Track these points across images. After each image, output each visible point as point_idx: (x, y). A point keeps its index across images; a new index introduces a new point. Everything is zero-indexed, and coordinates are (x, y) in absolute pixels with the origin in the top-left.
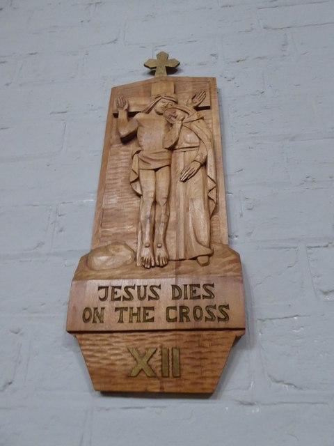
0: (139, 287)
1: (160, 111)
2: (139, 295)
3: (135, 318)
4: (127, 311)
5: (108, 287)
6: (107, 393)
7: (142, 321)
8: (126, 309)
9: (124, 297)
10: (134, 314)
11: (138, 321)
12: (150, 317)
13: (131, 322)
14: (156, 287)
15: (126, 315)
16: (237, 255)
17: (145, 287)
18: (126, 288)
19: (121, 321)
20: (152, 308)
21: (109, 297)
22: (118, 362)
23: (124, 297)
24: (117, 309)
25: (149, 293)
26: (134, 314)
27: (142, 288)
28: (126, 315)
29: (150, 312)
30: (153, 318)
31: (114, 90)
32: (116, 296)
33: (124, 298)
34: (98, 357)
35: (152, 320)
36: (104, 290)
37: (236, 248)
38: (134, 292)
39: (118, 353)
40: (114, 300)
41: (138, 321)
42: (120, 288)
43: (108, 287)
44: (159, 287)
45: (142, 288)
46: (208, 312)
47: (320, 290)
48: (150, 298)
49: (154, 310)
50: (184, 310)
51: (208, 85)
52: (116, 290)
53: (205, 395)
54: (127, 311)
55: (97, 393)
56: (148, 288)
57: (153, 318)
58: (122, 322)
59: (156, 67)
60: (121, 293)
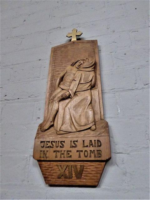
0: (56, 142)
1: (77, 67)
3: (62, 156)
4: (59, 152)
6: (51, 186)
7: (66, 157)
8: (58, 151)
9: (50, 146)
10: (62, 154)
13: (61, 157)
16: (107, 123)
19: (56, 157)
20: (71, 151)
22: (54, 174)
23: (60, 146)
24: (54, 151)
25: (60, 144)
26: (62, 154)
28: (82, 154)
29: (70, 153)
30: (71, 156)
32: (47, 146)
36: (43, 143)
37: (108, 120)
39: (57, 170)
41: (64, 157)
42: (49, 142)
44: (77, 141)
47: (96, 60)
48: (61, 147)
50: (99, 152)
51: (94, 43)
54: (59, 152)
55: (47, 185)
57: (71, 156)
58: (80, 157)
59: (72, 36)
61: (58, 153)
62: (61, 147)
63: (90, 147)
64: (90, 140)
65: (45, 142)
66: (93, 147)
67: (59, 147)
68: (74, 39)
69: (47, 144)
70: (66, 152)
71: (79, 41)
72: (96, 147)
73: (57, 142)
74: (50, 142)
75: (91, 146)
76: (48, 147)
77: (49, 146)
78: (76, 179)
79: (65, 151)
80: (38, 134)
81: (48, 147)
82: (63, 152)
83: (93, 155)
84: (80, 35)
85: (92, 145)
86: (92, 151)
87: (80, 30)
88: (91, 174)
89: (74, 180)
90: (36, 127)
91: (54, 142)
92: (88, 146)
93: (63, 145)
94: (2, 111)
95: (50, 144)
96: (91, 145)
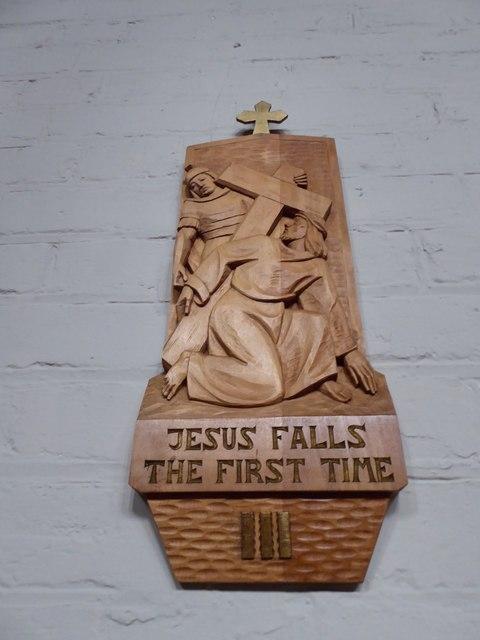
0: (225, 429)
2: (225, 440)
3: (175, 478)
4: (339, 463)
5: (182, 430)
6: (187, 586)
8: (337, 461)
9: (349, 442)
11: (180, 481)
12: (386, 474)
14: (359, 427)
15: (163, 470)
17: (234, 429)
18: (209, 430)
20: (200, 462)
21: (184, 446)
25: (240, 439)
26: (175, 472)
27: (229, 432)
29: (387, 465)
30: (200, 478)
31: (332, 140)
32: (193, 443)
33: (351, 444)
34: (364, 540)
35: (391, 477)
38: (219, 438)
40: (190, 448)
41: (180, 481)
42: (199, 430)
43: (182, 430)
44: (363, 428)
45: (229, 432)
46: (271, 468)
48: (241, 446)
49: (322, 459)
50: (253, 466)
52: (194, 434)
53: (350, 587)
56: (238, 431)
59: (254, 122)
60: (201, 438)
61: (158, 466)
64: (295, 427)
65: (185, 433)
66: (305, 447)
67: (237, 446)
68: (262, 128)
69: (194, 439)
70: (186, 463)
74: (203, 432)
75: (299, 446)
76: (198, 447)
79: (182, 461)
80: (147, 399)
81: (198, 447)
82: (176, 465)
83: (363, 474)
85: (302, 441)
87: (278, 109)
89: (253, 571)
90: (140, 387)
91: (217, 431)
92: (329, 446)
93: (248, 439)
94: (12, 25)
96: (299, 441)
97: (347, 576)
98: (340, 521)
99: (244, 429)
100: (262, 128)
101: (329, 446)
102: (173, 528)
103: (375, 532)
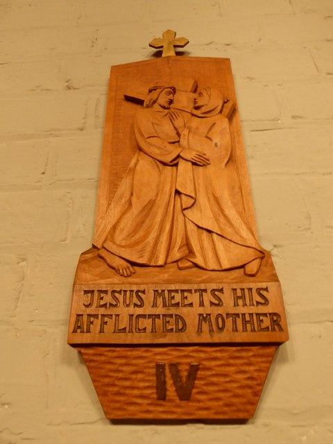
0: (125, 291)
2: (124, 302)
3: (240, 302)
4: (159, 318)
11: (245, 305)
18: (213, 290)
25: (135, 300)
42: (106, 292)
48: (135, 305)
51: (222, 67)
56: (254, 291)
59: (162, 47)
62: (135, 305)
63: (76, 332)
65: (96, 294)
71: (179, 57)
72: (242, 314)
73: (128, 293)
75: (79, 331)
76: (105, 305)
77: (106, 304)
78: (179, 364)
84: (183, 44)
86: (160, 291)
88: (213, 384)
89: (158, 412)
91: (120, 292)
92: (174, 330)
95: (108, 299)
96: (79, 327)
97: (241, 416)
98: (242, 365)
99: (259, 290)
100: (169, 53)
101: (174, 330)
102: (115, 364)
103: (267, 370)
